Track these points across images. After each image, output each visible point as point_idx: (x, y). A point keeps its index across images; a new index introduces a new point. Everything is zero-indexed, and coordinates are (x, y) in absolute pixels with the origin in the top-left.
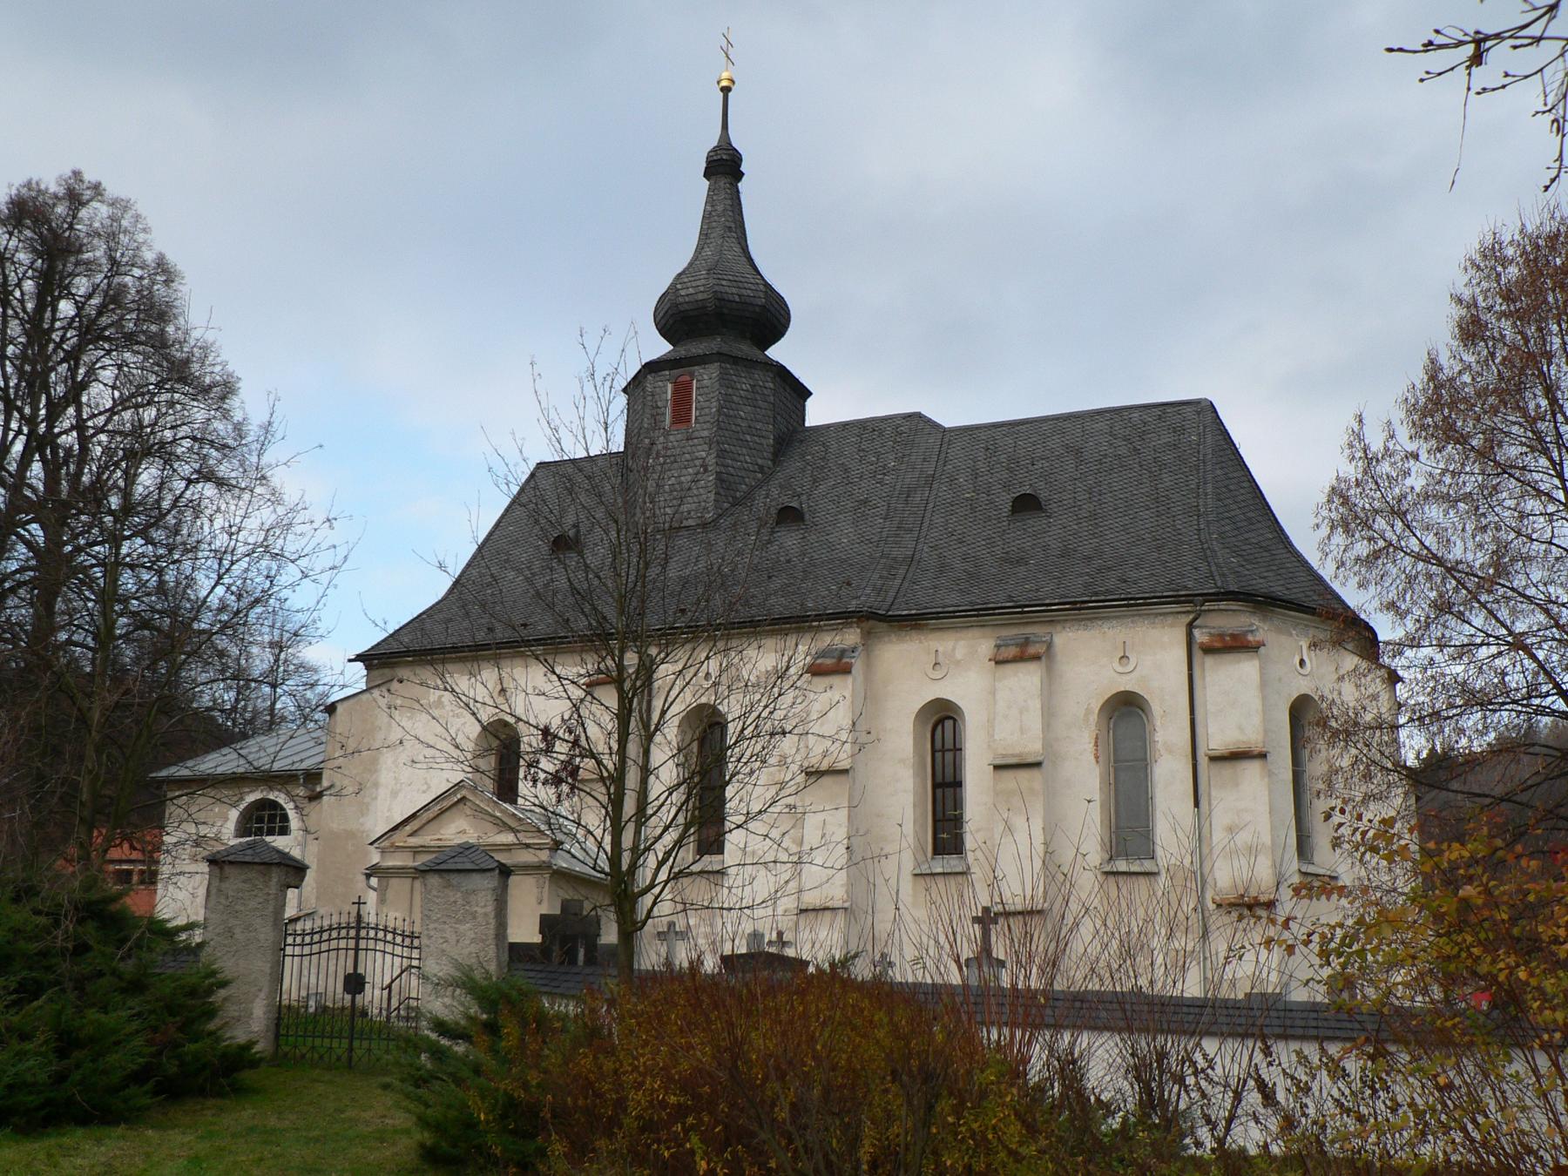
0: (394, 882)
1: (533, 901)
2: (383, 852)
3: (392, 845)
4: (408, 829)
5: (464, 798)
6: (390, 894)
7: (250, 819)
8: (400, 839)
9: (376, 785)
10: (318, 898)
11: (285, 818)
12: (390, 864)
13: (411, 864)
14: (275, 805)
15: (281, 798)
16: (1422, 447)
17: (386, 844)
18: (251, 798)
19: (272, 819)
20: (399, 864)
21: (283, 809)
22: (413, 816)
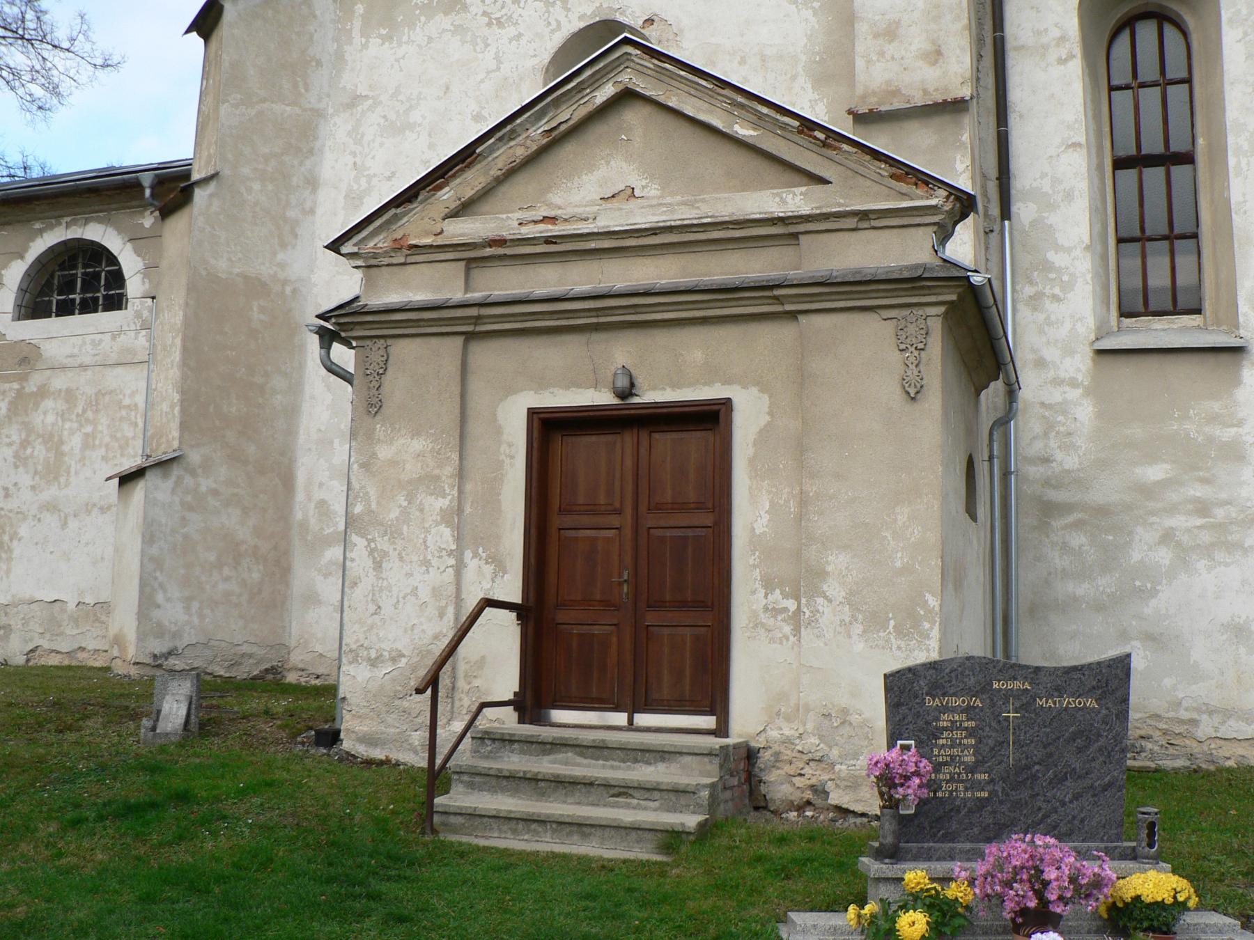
0: (406, 351)
1: (890, 392)
2: (370, 265)
3: (398, 246)
4: (447, 196)
5: (627, 96)
6: (396, 385)
7: (49, 284)
8: (419, 226)
9: (313, 183)
10: (183, 427)
11: (117, 278)
12: (393, 298)
13: (458, 296)
14: (98, 253)
15: (95, 232)
16: (1034, 185)
17: (381, 242)
18: (40, 245)
19: (90, 282)
20: (420, 296)
21: (113, 260)
22: (465, 157)
